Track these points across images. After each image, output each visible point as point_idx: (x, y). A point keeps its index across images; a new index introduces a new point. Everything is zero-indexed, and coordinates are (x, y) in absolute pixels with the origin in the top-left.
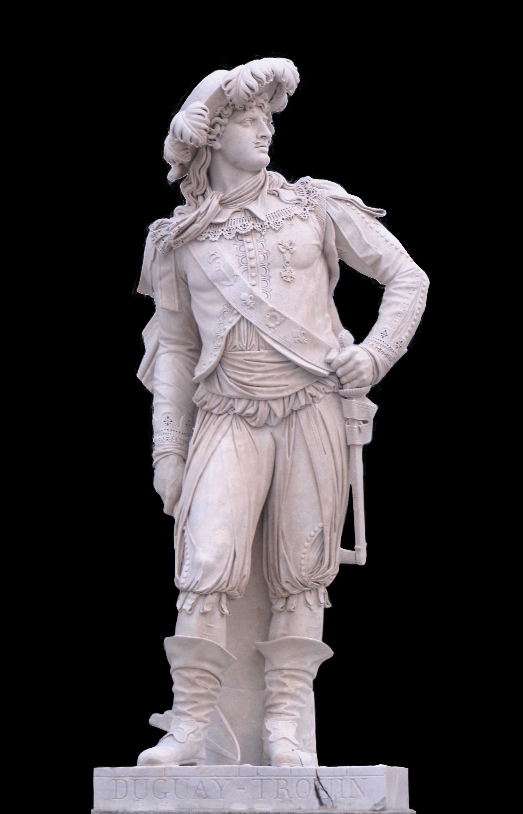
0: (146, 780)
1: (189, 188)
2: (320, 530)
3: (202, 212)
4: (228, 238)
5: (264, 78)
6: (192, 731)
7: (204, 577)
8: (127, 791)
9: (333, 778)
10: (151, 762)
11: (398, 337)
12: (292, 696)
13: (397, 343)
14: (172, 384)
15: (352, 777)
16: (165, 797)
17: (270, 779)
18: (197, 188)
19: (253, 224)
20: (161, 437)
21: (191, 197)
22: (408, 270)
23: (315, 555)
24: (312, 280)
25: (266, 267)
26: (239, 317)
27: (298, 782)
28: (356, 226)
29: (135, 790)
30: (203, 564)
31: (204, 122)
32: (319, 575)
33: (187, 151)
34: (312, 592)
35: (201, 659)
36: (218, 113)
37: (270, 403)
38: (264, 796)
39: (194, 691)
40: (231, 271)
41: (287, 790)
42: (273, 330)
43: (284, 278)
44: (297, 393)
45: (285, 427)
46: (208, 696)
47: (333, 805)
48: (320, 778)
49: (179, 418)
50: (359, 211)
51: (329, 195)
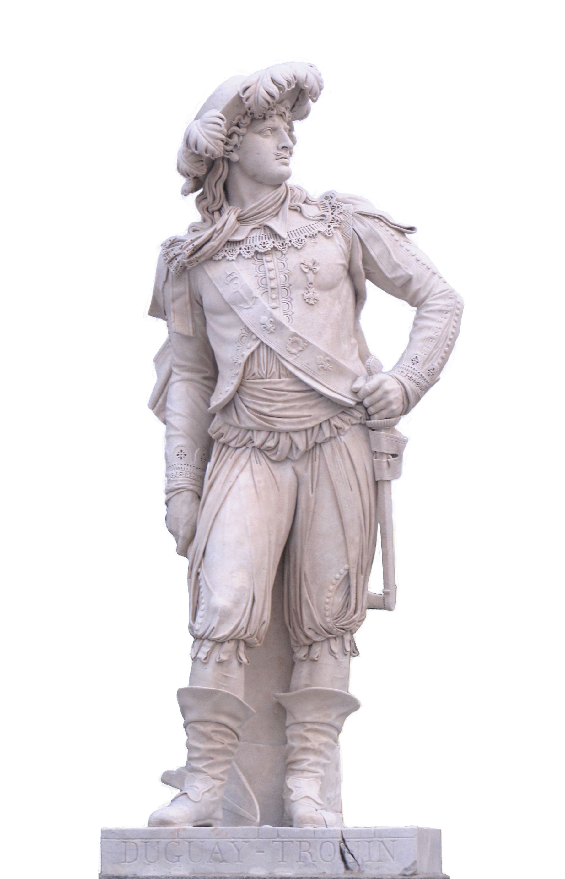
0: (158, 842)
2: (346, 573)
3: (218, 229)
4: (246, 257)
5: (285, 84)
6: (207, 789)
7: (221, 623)
8: (137, 855)
9: (359, 840)
11: (430, 364)
12: (315, 752)
13: (429, 371)
14: (185, 415)
15: (380, 839)
16: (179, 861)
17: (292, 842)
18: (213, 203)
19: (273, 242)
20: (174, 472)
21: (206, 212)
22: (441, 292)
23: (340, 599)
24: (337, 303)
25: (288, 288)
26: (258, 343)
27: (322, 844)
28: (384, 244)
29: (146, 854)
30: (219, 609)
31: (221, 132)
32: (344, 621)
33: (202, 163)
34: (337, 639)
35: (217, 711)
36: (235, 122)
37: (292, 435)
38: (285, 860)
39: (210, 746)
40: (250, 292)
41: (310, 853)
42: (295, 356)
43: (307, 301)
44: (320, 425)
45: (308, 461)
46: (225, 752)
47: (359, 870)
48: (346, 840)
49: (193, 452)
50: (388, 228)
51: (356, 211)
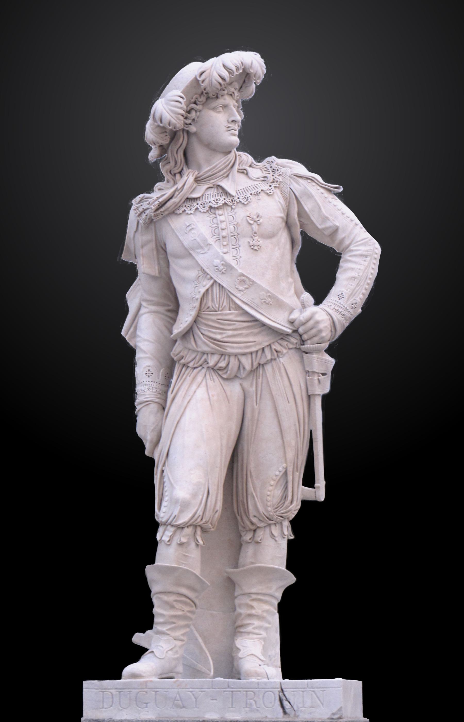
0: (130, 692)
1: (168, 167)
2: (284, 470)
3: (179, 188)
4: (202, 211)
5: (234, 69)
6: (170, 648)
7: (181, 511)
8: (113, 702)
9: (295, 690)
10: (134, 676)
11: (353, 299)
12: (259, 617)
13: (352, 304)
14: (152, 341)
15: (312, 690)
16: (147, 707)
17: (240, 691)
18: (175, 167)
19: (225, 199)
20: (143, 388)
21: (169, 174)
22: (362, 240)
23: (280, 492)
24: (277, 249)
25: (236, 237)
26: (212, 282)
27: (264, 693)
28: (316, 201)
29: (120, 701)
30: (180, 501)
31: (181, 108)
32: (283, 510)
33: (166, 134)
34: (277, 525)
35: (178, 584)
36: (193, 100)
37: (240, 357)
38: (234, 706)
39: (173, 613)
40: (205, 240)
41: (254, 700)
42: (242, 293)
43: (252, 247)
44: (263, 349)
45: (253, 379)
46: (184, 617)
47: (295, 714)
48: (284, 690)
49: (159, 371)
50: (319, 188)
51: (292, 173)
